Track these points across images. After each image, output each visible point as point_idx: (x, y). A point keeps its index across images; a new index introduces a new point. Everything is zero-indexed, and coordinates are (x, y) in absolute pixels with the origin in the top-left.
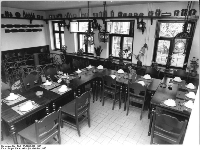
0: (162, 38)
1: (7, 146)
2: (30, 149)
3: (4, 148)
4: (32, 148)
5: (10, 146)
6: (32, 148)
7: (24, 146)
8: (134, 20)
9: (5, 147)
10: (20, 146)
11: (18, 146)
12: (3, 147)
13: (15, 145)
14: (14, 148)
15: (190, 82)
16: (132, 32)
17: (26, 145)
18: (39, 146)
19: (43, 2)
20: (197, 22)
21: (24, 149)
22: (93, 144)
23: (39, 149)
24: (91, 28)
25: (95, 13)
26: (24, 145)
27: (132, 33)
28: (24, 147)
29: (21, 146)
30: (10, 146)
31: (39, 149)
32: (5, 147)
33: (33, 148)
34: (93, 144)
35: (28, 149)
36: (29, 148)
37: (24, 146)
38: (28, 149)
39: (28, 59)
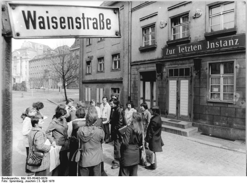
0: (220, 108)
1: (9, 178)
3: (4, 180)
5: (12, 179)
8: (224, 99)
9: (6, 180)
10: (25, 178)
11: (22, 178)
13: (18, 177)
14: (24, 180)
20: (245, 101)
21: (29, 181)
22: (112, 45)
24: (144, 137)
28: (30, 180)
29: (26, 178)
30: (12, 179)
32: (6, 180)
34: (112, 45)
35: (36, 181)
36: (38, 180)
38: (36, 181)
39: (231, 37)
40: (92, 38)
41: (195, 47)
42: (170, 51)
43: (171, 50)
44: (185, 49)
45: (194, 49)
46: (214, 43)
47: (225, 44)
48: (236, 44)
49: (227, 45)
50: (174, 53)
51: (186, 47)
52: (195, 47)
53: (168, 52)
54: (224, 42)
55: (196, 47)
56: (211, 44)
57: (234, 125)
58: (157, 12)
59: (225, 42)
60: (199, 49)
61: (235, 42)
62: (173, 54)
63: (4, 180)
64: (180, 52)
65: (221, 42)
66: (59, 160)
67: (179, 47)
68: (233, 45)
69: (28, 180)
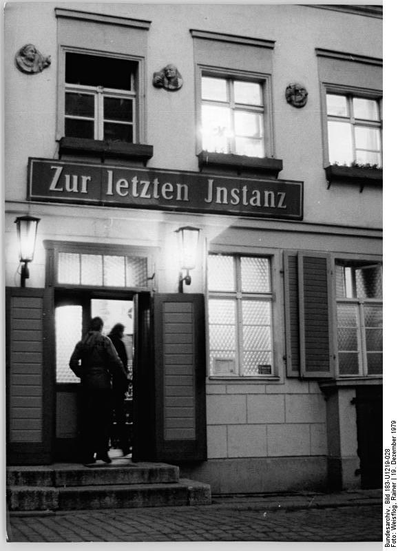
1: (388, 532)
2: (394, 471)
3: (391, 541)
4: (392, 467)
6: (392, 467)
7: (387, 485)
9: (391, 538)
12: (390, 544)
15: (119, 448)
16: (28, 387)
17: (385, 493)
18: (387, 474)
19: (36, 541)
23: (394, 487)
25: (18, 472)
26: (384, 485)
27: (39, 161)
29: (387, 493)
30: (388, 524)
31: (394, 487)
32: (391, 538)
33: (394, 463)
37: (387, 485)
40: (354, 145)
41: (168, 187)
42: (68, 177)
43: (75, 177)
44: (130, 184)
45: (164, 195)
46: (225, 191)
47: (255, 201)
48: (280, 205)
49: (258, 204)
50: (84, 190)
51: (135, 181)
52: (168, 187)
53: (61, 182)
54: (253, 193)
55: (171, 189)
56: (219, 189)
57: (127, 423)
58: (150, 22)
59: (256, 193)
60: (179, 198)
61: (148, 189)
62: (79, 194)
63: (391, 541)
64: (110, 192)
65: (245, 189)
66: (357, 443)
67: (110, 173)
68: (186, 201)
69: (391, 488)
